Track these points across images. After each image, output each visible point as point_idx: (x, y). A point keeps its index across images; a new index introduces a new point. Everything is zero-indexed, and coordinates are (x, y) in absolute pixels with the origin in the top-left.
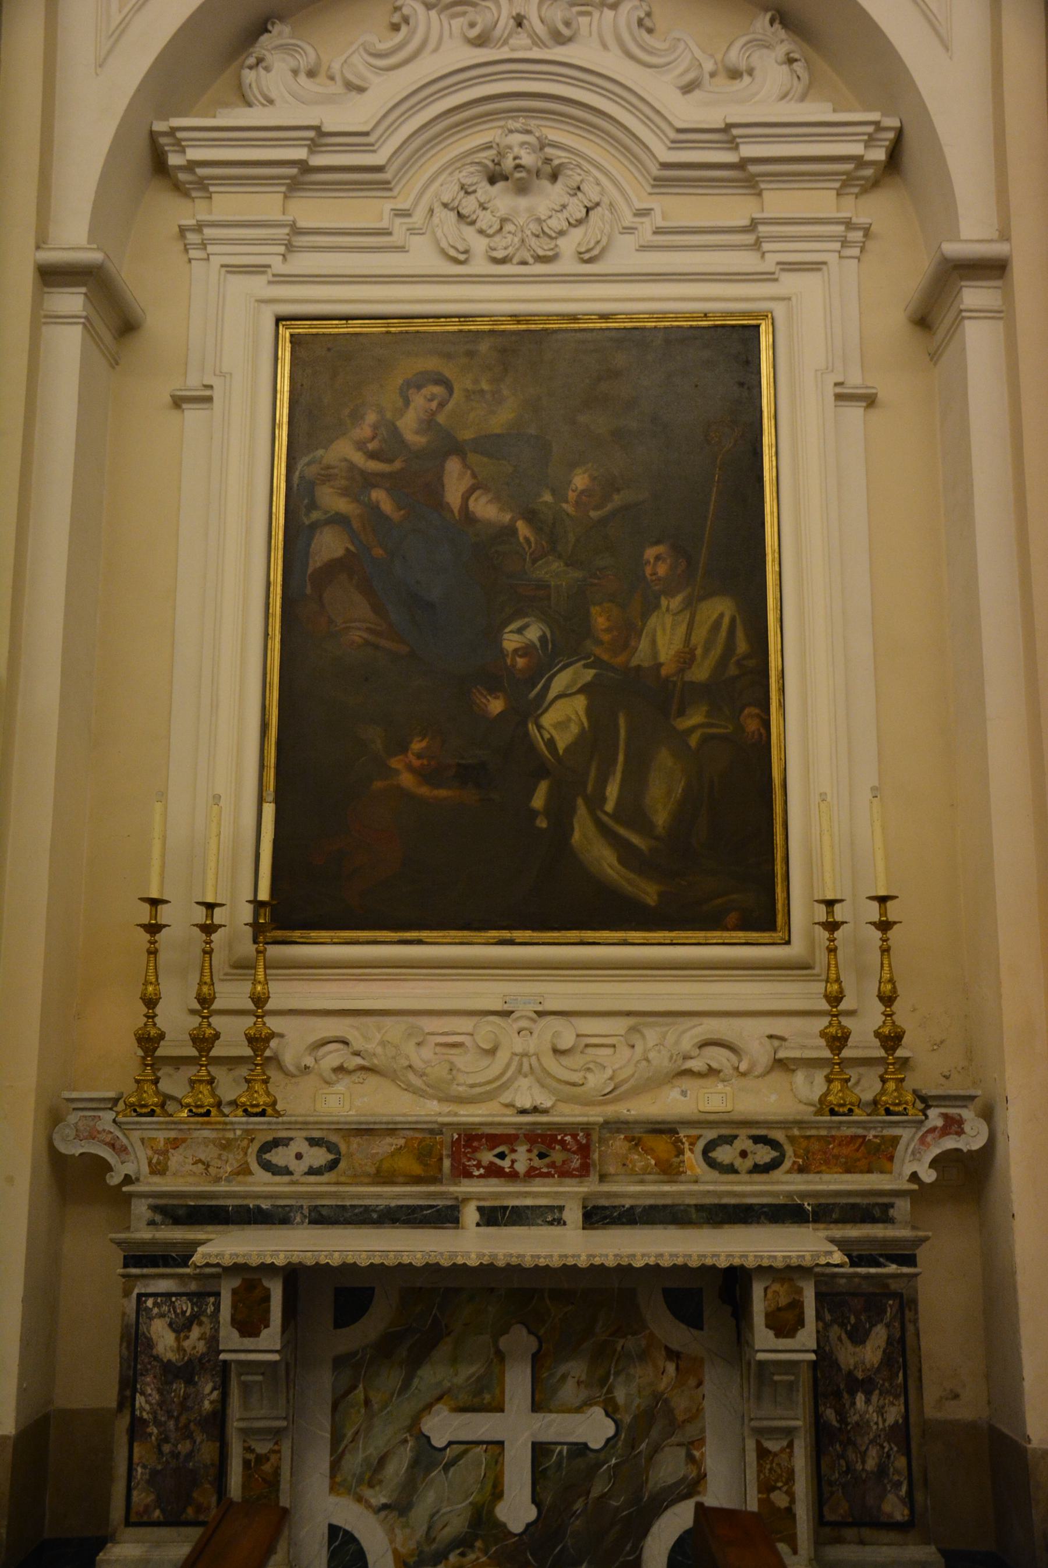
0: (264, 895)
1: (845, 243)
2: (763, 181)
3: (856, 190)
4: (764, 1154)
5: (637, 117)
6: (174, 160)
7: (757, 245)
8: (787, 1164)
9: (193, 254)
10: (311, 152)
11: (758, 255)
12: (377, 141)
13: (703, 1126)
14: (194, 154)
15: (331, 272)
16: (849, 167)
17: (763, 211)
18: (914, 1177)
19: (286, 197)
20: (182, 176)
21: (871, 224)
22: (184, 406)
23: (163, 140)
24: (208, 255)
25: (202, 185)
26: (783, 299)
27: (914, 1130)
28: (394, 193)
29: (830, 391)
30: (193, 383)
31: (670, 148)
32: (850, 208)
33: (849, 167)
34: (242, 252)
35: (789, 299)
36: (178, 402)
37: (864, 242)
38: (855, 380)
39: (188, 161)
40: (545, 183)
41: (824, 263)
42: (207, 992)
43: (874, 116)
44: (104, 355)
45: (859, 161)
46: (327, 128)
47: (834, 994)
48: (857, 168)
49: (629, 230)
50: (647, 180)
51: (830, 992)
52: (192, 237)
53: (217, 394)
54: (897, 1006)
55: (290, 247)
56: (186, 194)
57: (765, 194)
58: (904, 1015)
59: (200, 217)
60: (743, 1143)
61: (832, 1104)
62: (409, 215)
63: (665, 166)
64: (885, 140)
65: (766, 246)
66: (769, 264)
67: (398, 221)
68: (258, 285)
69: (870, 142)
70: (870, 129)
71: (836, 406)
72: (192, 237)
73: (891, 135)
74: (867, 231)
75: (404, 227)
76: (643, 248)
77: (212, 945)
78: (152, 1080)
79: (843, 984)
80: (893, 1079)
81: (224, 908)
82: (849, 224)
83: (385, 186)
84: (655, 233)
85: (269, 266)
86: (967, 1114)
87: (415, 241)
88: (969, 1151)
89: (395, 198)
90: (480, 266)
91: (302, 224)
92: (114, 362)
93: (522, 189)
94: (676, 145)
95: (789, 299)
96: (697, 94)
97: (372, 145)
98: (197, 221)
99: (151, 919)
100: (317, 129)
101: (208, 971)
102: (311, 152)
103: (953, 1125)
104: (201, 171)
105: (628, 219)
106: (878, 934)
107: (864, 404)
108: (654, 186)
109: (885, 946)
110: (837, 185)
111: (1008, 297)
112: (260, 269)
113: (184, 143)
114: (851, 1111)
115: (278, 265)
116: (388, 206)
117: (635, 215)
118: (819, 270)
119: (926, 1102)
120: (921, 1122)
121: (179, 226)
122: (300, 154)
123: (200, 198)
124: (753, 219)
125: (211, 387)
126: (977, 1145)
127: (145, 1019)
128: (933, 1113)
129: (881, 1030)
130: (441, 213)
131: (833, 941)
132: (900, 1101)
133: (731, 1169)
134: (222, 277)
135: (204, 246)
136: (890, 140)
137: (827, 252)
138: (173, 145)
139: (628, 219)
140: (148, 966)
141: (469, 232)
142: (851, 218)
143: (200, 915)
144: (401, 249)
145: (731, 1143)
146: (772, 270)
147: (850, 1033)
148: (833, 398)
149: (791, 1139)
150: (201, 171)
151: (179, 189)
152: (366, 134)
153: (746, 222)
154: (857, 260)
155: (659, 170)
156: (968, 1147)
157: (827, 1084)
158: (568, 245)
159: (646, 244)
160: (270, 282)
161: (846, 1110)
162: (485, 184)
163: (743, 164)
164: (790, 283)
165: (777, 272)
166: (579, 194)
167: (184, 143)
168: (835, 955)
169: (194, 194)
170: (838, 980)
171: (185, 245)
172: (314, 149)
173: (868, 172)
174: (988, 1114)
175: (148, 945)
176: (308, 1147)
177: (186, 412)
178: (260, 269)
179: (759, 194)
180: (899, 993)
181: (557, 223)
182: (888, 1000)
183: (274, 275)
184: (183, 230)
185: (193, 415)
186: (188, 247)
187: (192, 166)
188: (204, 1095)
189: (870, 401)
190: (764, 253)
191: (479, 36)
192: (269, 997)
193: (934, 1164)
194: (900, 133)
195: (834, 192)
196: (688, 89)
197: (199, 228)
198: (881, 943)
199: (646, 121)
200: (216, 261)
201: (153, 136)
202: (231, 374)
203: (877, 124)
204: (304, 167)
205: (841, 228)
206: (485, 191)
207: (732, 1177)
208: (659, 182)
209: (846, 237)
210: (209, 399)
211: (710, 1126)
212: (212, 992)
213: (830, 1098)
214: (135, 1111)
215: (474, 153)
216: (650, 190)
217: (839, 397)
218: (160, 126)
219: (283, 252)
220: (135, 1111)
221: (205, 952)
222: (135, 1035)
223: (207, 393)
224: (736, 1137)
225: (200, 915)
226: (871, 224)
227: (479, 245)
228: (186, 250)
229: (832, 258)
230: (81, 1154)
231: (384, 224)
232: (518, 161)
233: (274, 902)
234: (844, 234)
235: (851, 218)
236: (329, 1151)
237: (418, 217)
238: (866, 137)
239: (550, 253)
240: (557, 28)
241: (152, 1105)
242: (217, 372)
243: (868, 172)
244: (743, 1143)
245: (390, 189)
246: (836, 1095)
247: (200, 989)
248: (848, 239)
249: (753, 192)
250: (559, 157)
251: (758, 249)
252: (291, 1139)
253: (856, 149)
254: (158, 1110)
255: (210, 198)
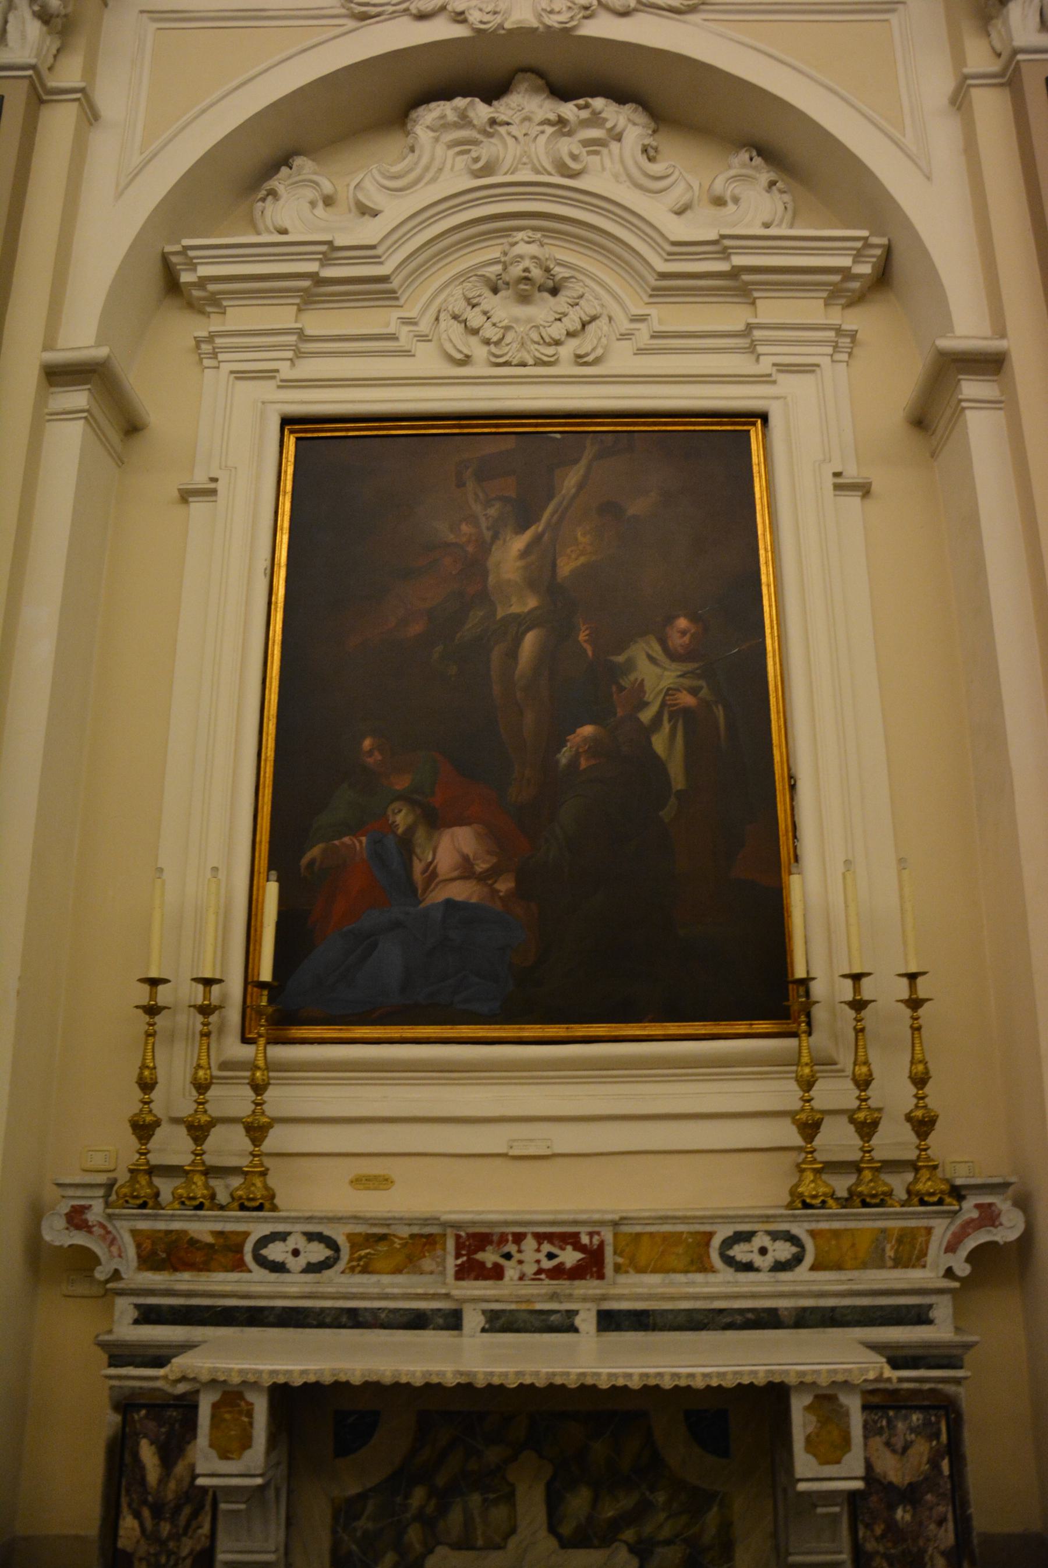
0: (266, 974)
1: (836, 347)
2: (756, 290)
3: (843, 301)
4: (318, 1252)
5: (636, 234)
6: (186, 277)
7: (752, 349)
8: (342, 1264)
9: (207, 362)
10: (322, 265)
11: (753, 357)
12: (384, 253)
13: (891, 1217)
14: (204, 271)
15: (319, 377)
16: (836, 278)
17: (756, 317)
18: (949, 1273)
19: (300, 310)
20: (196, 293)
21: (857, 331)
22: (191, 499)
23: (174, 259)
24: (219, 362)
25: (214, 300)
26: (777, 398)
27: (949, 1220)
28: (402, 302)
29: (830, 481)
30: (200, 480)
31: (667, 260)
32: (835, 316)
33: (836, 278)
34: (260, 358)
35: (785, 398)
36: (186, 496)
37: (852, 348)
38: (852, 473)
39: (199, 277)
40: (546, 295)
41: (818, 366)
42: (203, 1077)
43: (865, 233)
44: (110, 454)
45: (845, 273)
46: (339, 243)
47: (919, 1075)
48: (843, 280)
49: (625, 336)
50: (646, 292)
51: (916, 1073)
52: (205, 347)
53: (220, 486)
54: (928, 1089)
55: (299, 354)
56: (202, 312)
57: (758, 301)
58: (935, 1096)
59: (212, 329)
60: (296, 1241)
61: (863, 1195)
62: (415, 324)
63: (663, 276)
64: (873, 256)
65: (760, 349)
66: (765, 366)
67: (406, 329)
68: (267, 390)
69: (858, 256)
70: (859, 244)
71: (835, 495)
72: (205, 347)
73: (878, 252)
74: (853, 335)
75: (412, 334)
76: (641, 351)
77: (156, 1027)
78: (201, 1171)
79: (928, 1064)
80: (868, 1168)
81: (841, 973)
82: (839, 331)
83: (391, 296)
84: (653, 337)
85: (277, 371)
86: (1003, 1204)
87: (421, 348)
88: (1006, 1243)
89: (402, 307)
90: (479, 369)
91: (309, 332)
92: (120, 461)
93: (524, 299)
94: (671, 257)
95: (785, 398)
96: (689, 214)
97: (379, 257)
98: (210, 332)
99: (204, 1000)
100: (329, 243)
101: (150, 1054)
102: (322, 265)
103: (989, 1217)
104: (212, 287)
105: (625, 325)
106: (852, 1014)
107: (860, 493)
108: (651, 296)
109: (859, 1026)
110: (825, 295)
111: (1010, 392)
112: (269, 375)
113: (195, 261)
114: (824, 1202)
115: (286, 371)
116: (396, 314)
117: (632, 321)
118: (813, 371)
119: (958, 1193)
120: (956, 1213)
121: (195, 338)
122: (312, 267)
123: (215, 313)
124: (748, 324)
125: (214, 480)
126: (1012, 1236)
127: (141, 1105)
128: (969, 1204)
129: (913, 1114)
130: (446, 322)
131: (917, 1019)
132: (818, 1193)
133: (748, 1267)
134: (231, 382)
135: (214, 355)
136: (879, 257)
137: (820, 355)
138: (185, 264)
139: (625, 325)
140: (145, 1049)
141: (474, 340)
142: (840, 325)
143: (142, 994)
144: (407, 353)
145: (284, 1240)
146: (768, 372)
147: (938, 1116)
148: (832, 487)
149: (813, 1234)
150: (212, 287)
151: (192, 306)
152: (373, 247)
153: (740, 327)
154: (845, 364)
155: (656, 280)
156: (1004, 1239)
157: (798, 1174)
158: (566, 351)
159: (643, 347)
160: (279, 387)
161: (877, 1201)
162: (488, 293)
163: (736, 273)
164: (788, 383)
165: (774, 375)
166: (470, 308)
167: (195, 261)
168: (920, 1033)
169: (209, 309)
170: (866, 1063)
171: (200, 354)
172: (325, 262)
173: (856, 285)
174: (1024, 1203)
175: (147, 1027)
176: (306, 1242)
177: (192, 505)
178: (269, 375)
179: (753, 303)
180: (874, 1076)
181: (557, 331)
182: (920, 1081)
183: (282, 381)
184: (198, 342)
185: (198, 507)
186: (202, 356)
187: (203, 282)
188: (197, 1187)
189: (864, 490)
190: (759, 355)
191: (482, 169)
192: (156, 1083)
193: (969, 1259)
194: (889, 250)
195: (822, 302)
196: (679, 213)
197: (211, 338)
198: (854, 1023)
199: (645, 237)
200: (225, 368)
201: (165, 258)
202: (236, 468)
203: (866, 239)
204: (318, 280)
205: (831, 334)
206: (489, 301)
207: (751, 1276)
208: (657, 292)
209: (837, 342)
210: (213, 492)
211: (926, 1216)
212: (208, 1077)
213: (800, 1190)
214: (183, 1203)
215: (484, 266)
216: (647, 300)
217: (837, 487)
218: (168, 249)
219: (290, 357)
220: (183, 1203)
221: (149, 1035)
222: (130, 1121)
223: (212, 486)
224: (289, 1234)
225: (142, 994)
226: (857, 331)
227: (480, 352)
228: (201, 360)
229: (825, 361)
230: (71, 1246)
231: (391, 330)
232: (526, 274)
233: (276, 984)
234: (836, 339)
235: (840, 325)
236: (328, 1246)
237: (424, 326)
238: (854, 252)
239: (552, 359)
240: (561, 158)
241: (144, 1197)
242: (233, 470)
243: (856, 285)
244: (296, 1241)
245: (397, 299)
246: (808, 1186)
247: (141, 1073)
248: (840, 345)
249: (746, 301)
250: (560, 272)
251: (752, 352)
252: (289, 1234)
253: (845, 262)
254: (207, 1203)
255: (224, 313)
